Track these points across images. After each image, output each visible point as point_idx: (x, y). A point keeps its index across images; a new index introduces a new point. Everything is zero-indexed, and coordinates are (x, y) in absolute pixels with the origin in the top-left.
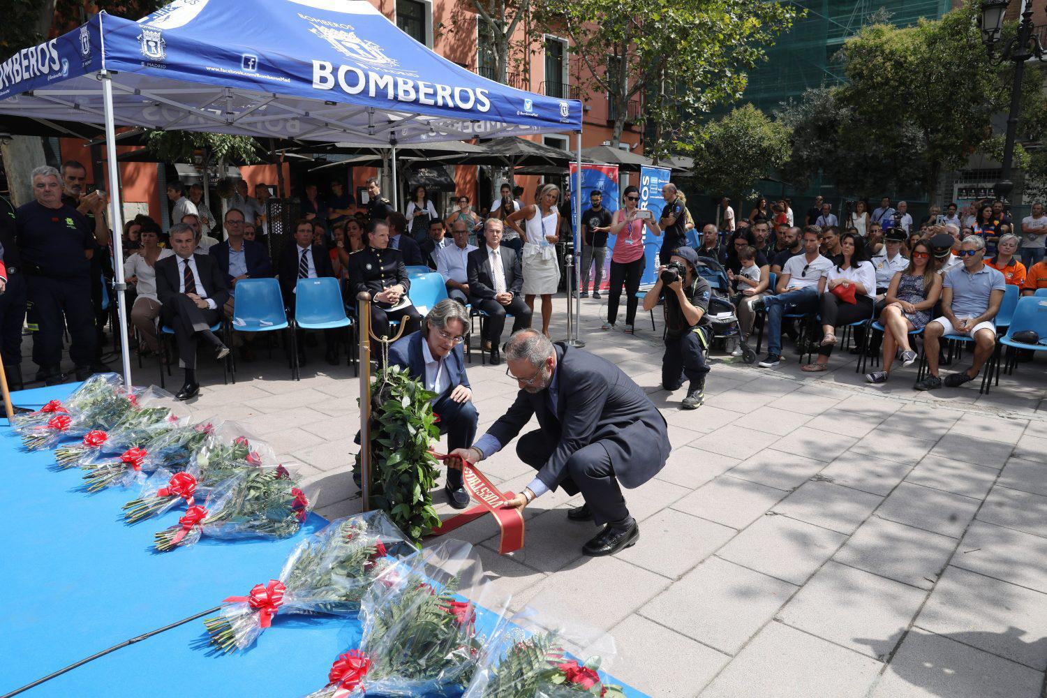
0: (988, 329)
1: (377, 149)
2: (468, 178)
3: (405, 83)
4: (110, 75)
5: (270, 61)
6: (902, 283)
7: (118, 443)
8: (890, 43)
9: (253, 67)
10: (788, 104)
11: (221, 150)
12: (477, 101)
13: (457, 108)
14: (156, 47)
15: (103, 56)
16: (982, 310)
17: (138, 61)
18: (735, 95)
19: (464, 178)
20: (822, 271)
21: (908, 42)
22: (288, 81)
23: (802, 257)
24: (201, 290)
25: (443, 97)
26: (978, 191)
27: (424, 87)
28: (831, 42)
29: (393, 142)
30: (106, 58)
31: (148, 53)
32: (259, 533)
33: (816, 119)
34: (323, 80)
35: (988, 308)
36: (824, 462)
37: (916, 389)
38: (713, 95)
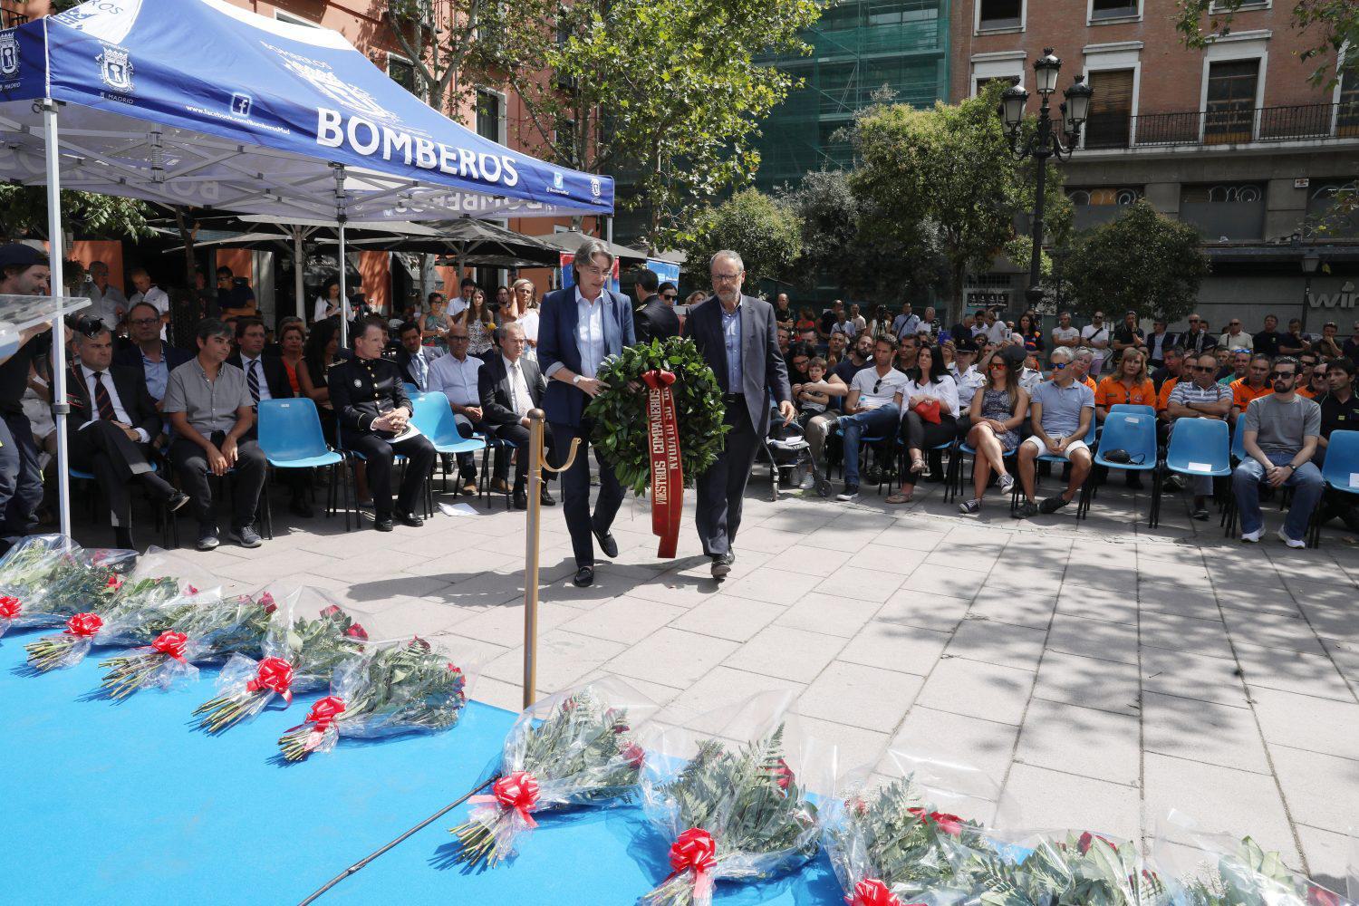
0: (1081, 448)
1: (289, 227)
2: (377, 268)
3: (425, 145)
4: (57, 107)
5: (267, 105)
6: (987, 400)
7: (118, 630)
8: (912, 127)
9: (245, 111)
10: (784, 189)
11: (98, 219)
12: (504, 172)
13: (482, 181)
14: (120, 72)
15: (48, 79)
16: (1074, 428)
17: (96, 91)
18: (746, 176)
19: (372, 268)
20: (897, 387)
21: (930, 127)
22: (287, 132)
23: (872, 370)
24: (123, 418)
25: (467, 165)
26: (987, 297)
27: (399, 144)
28: (824, 118)
29: (342, 218)
30: (52, 83)
31: (110, 80)
32: (418, 724)
33: (819, 208)
34: (330, 134)
35: (1079, 424)
36: (972, 602)
37: (1015, 517)
38: (721, 175)
